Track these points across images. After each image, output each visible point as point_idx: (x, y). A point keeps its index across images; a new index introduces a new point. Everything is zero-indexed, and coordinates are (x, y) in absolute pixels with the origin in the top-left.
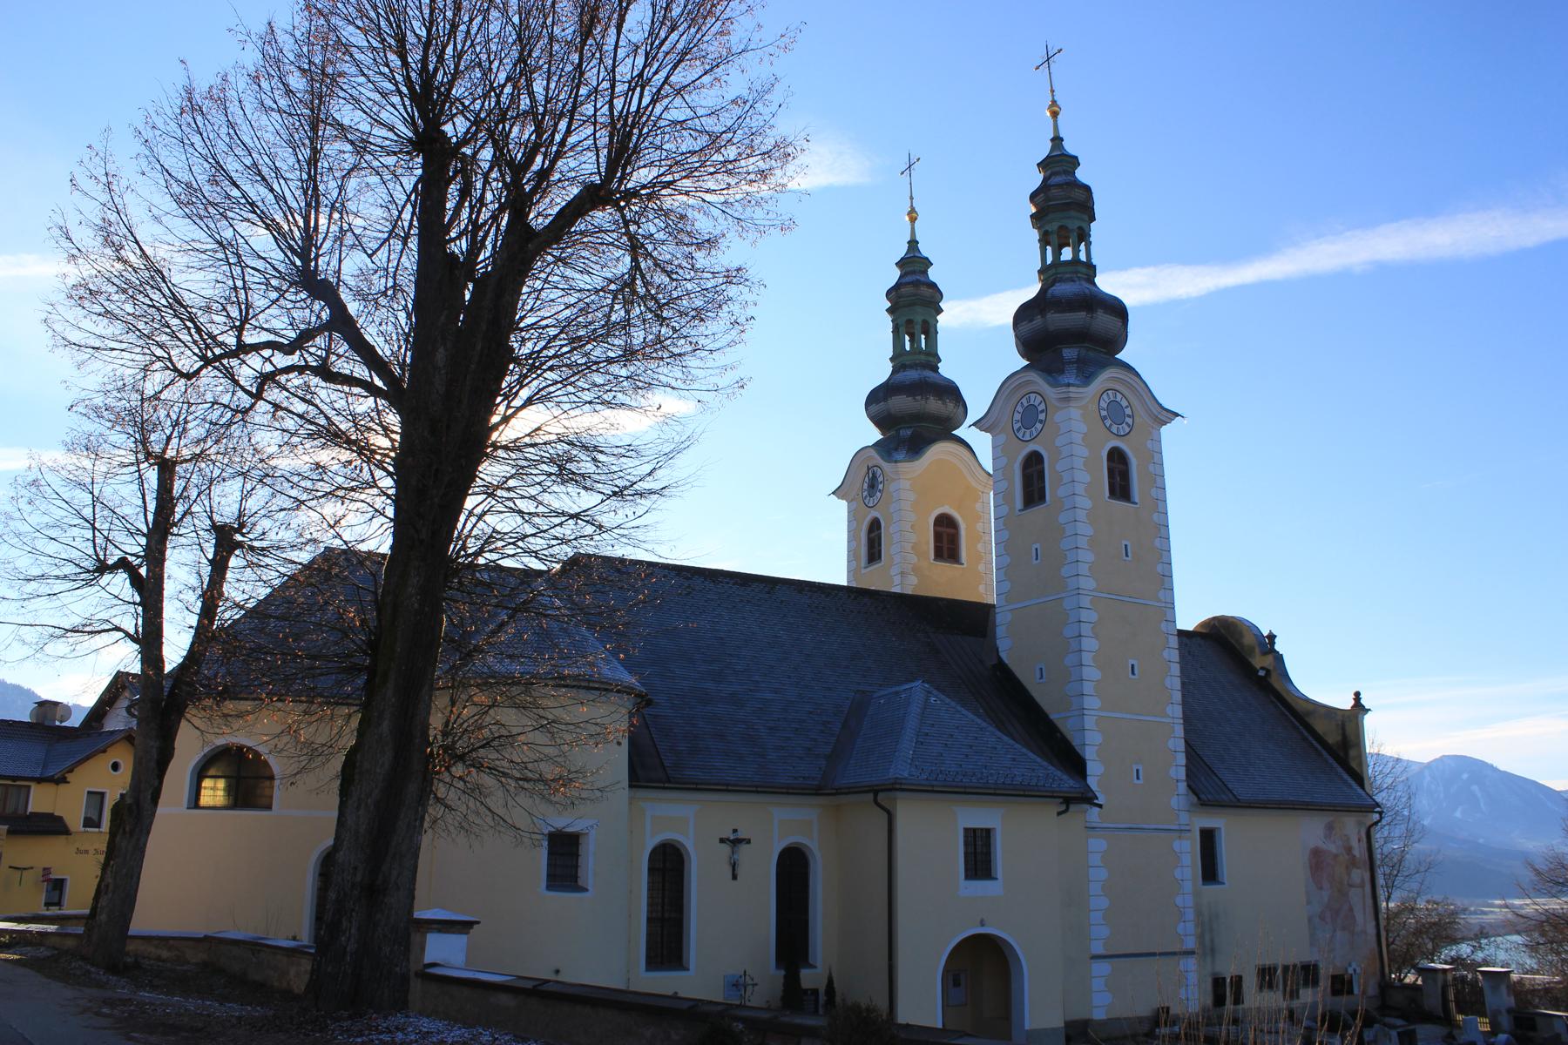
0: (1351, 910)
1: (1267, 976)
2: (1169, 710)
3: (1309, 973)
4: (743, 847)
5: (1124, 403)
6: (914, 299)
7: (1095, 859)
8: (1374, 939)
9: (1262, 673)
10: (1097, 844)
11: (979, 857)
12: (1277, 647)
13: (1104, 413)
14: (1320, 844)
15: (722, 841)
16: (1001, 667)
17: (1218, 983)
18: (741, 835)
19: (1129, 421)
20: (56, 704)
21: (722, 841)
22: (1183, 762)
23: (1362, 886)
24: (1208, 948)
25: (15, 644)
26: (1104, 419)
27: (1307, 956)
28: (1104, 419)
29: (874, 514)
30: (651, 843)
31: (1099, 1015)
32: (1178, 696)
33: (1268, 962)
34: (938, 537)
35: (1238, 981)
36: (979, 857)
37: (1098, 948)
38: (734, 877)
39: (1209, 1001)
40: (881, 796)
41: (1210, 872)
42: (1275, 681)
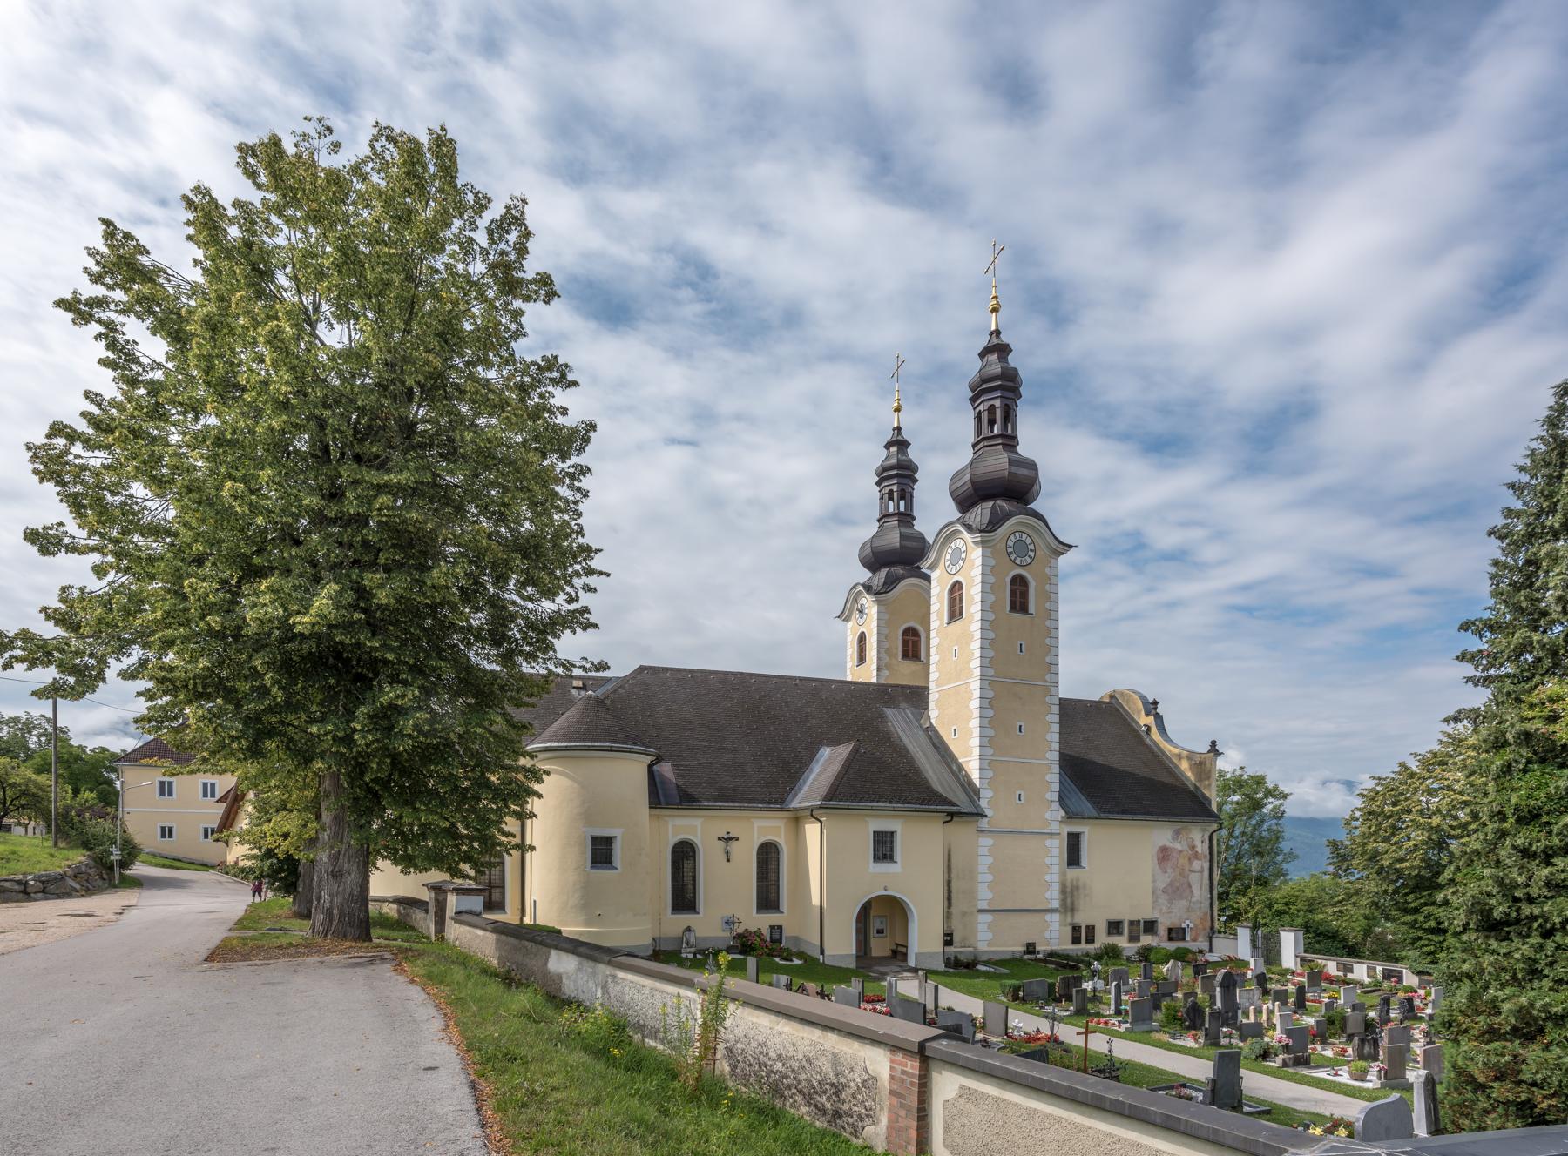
1: (1115, 927)
3: (1150, 927)
4: (734, 844)
5: (1028, 541)
6: (899, 475)
7: (984, 851)
10: (985, 842)
11: (884, 847)
14: (1168, 844)
17: (1076, 929)
20: (951, 493)
23: (1202, 872)
25: (830, 640)
26: (1009, 554)
27: (1149, 916)
28: (1009, 554)
29: (862, 629)
30: (673, 840)
33: (1115, 917)
34: (905, 643)
35: (1091, 930)
36: (884, 847)
41: (1074, 858)
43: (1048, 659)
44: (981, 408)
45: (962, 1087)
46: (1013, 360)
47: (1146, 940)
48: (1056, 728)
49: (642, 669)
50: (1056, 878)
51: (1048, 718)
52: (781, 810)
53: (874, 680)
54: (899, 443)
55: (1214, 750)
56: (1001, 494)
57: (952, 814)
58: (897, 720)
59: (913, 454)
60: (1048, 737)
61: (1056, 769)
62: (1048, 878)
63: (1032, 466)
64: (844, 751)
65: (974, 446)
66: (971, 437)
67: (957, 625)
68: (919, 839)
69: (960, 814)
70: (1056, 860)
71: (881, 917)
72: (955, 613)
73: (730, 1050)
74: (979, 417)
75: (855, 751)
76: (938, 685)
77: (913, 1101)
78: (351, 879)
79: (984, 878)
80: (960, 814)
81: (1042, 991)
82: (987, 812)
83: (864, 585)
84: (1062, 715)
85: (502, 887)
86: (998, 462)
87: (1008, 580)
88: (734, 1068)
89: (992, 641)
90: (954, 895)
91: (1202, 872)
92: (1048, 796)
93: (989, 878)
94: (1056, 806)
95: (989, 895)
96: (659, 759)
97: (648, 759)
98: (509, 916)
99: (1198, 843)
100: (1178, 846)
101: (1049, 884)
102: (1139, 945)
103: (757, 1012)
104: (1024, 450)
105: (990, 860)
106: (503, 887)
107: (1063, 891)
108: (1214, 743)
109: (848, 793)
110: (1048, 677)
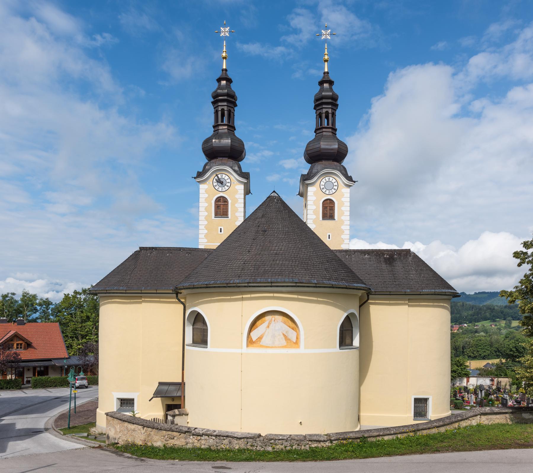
34: (217, 207)
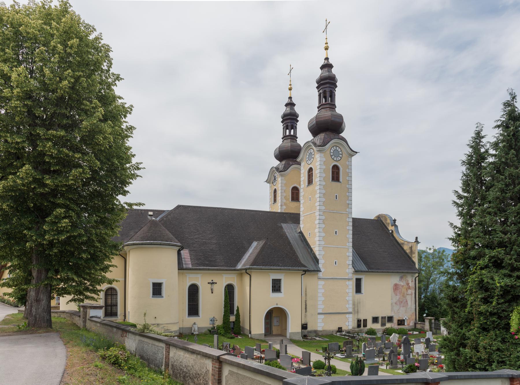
0: (407, 301)
1: (375, 320)
2: (348, 244)
5: (339, 150)
6: (290, 120)
8: (414, 310)
9: (391, 232)
10: (321, 283)
11: (276, 287)
12: (396, 224)
13: (332, 154)
14: (398, 283)
15: (209, 283)
16: (301, 233)
17: (359, 321)
18: (214, 281)
19: (341, 156)
21: (209, 283)
22: (351, 259)
23: (412, 295)
24: (356, 310)
25: (254, 194)
26: (331, 156)
27: (390, 315)
28: (342, 154)
29: (275, 187)
31: (320, 329)
32: (351, 240)
34: (293, 193)
35: (365, 321)
36: (276, 287)
37: (320, 311)
38: (212, 293)
39: (356, 325)
40: (248, 271)
41: (358, 289)
42: (395, 235)
43: (348, 202)
44: (321, 91)
45: (229, 370)
46: (334, 71)
47: (388, 325)
48: (351, 232)
49: (179, 207)
50: (351, 298)
51: (348, 228)
52: (235, 270)
53: (279, 211)
54: (290, 104)
55: (417, 241)
56: (329, 128)
57: (305, 271)
58: (287, 228)
59: (297, 109)
60: (348, 236)
61: (351, 250)
62: (347, 298)
63: (341, 117)
64: (262, 243)
65: (318, 108)
66: (317, 104)
67: (311, 187)
68: (291, 283)
69: (308, 271)
70: (351, 291)
71: (275, 317)
72: (310, 181)
73: (172, 365)
74: (320, 95)
75: (265, 244)
76: (303, 214)
77: (217, 377)
78: (44, 302)
79: (321, 299)
80: (308, 271)
81: (336, 348)
82: (322, 270)
83: (276, 168)
84: (353, 226)
85: (116, 305)
86: (327, 114)
87: (331, 167)
88: (173, 372)
89: (324, 194)
90: (308, 307)
91: (412, 295)
92: (347, 262)
93: (323, 299)
94: (351, 266)
95: (323, 307)
96: (182, 248)
97: (178, 248)
98: (119, 319)
99: (410, 282)
100: (402, 284)
101: (348, 301)
102: (385, 327)
103: (180, 350)
104: (338, 110)
105: (323, 291)
106: (117, 306)
107: (354, 304)
108: (417, 238)
109: (263, 262)
110: (347, 210)
